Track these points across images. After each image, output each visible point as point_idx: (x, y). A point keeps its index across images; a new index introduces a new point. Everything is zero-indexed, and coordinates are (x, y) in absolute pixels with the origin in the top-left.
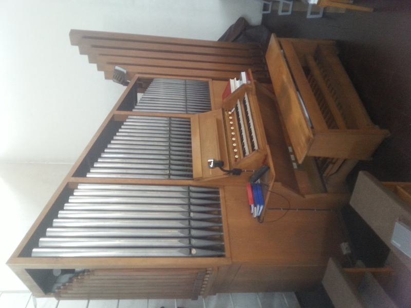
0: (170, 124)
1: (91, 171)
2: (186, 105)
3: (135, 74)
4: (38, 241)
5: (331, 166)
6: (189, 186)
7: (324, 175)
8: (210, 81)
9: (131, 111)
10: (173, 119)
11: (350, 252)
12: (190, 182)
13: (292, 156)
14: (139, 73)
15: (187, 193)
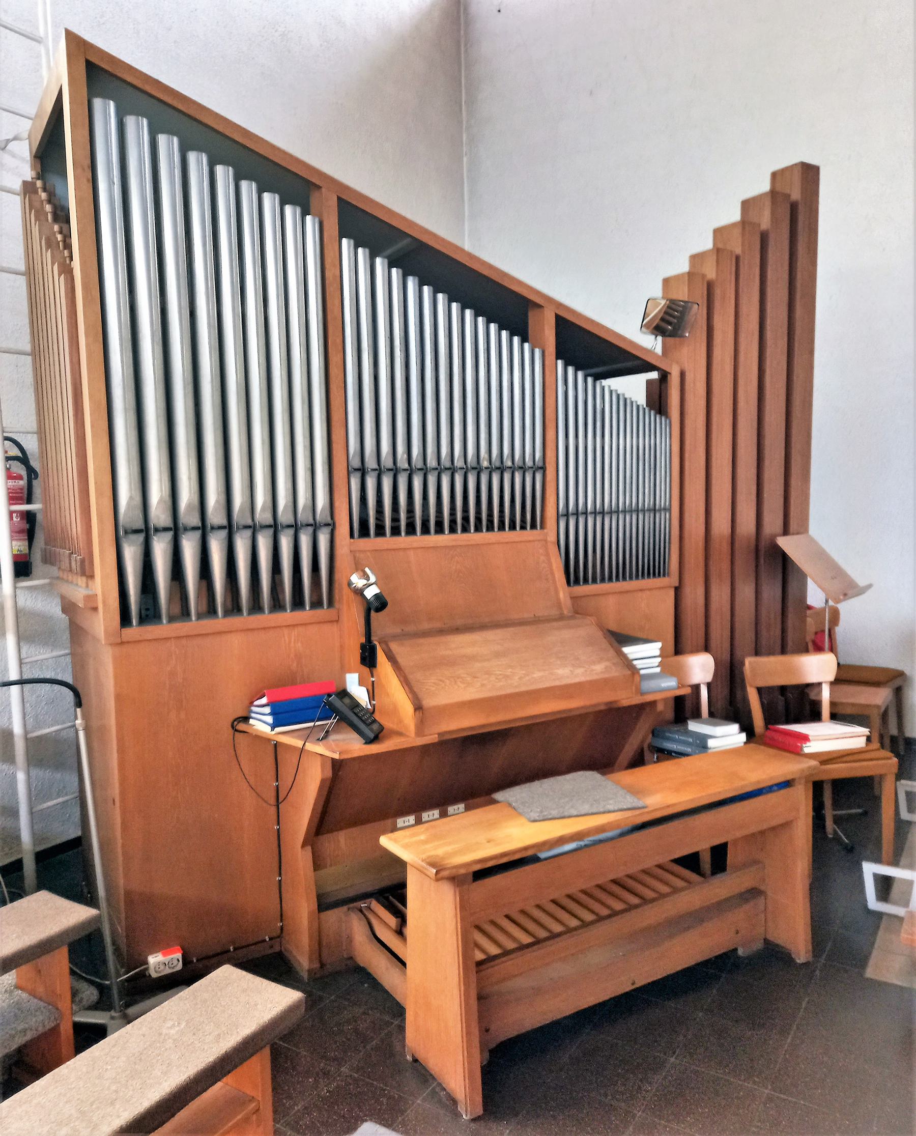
0: (523, 469)
1: (360, 250)
2: (603, 513)
3: (677, 363)
4: (143, 116)
5: (392, 921)
6: (332, 526)
7: (375, 905)
8: (673, 580)
9: (558, 357)
10: (539, 477)
11: (154, 975)
12: (343, 529)
13: (411, 819)
14: (682, 375)
15: (311, 521)
